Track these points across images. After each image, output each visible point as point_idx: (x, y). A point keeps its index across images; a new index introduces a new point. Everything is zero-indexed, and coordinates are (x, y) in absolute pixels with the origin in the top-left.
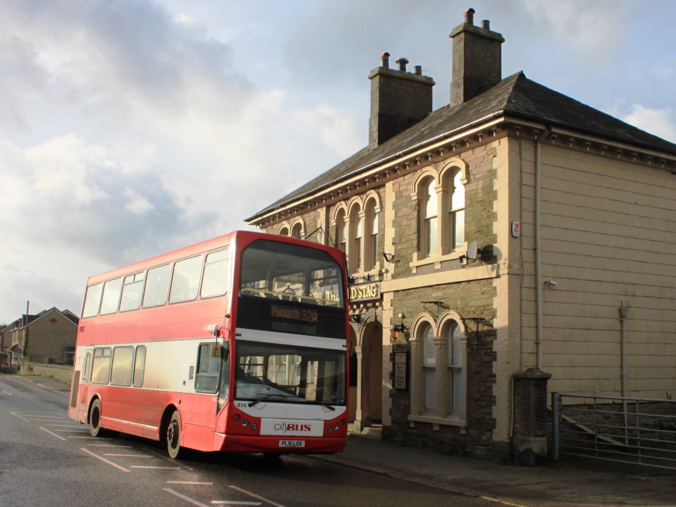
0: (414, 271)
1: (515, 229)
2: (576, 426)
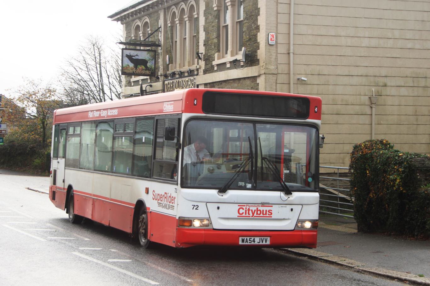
0: (216, 68)
1: (271, 39)
2: (326, 190)
